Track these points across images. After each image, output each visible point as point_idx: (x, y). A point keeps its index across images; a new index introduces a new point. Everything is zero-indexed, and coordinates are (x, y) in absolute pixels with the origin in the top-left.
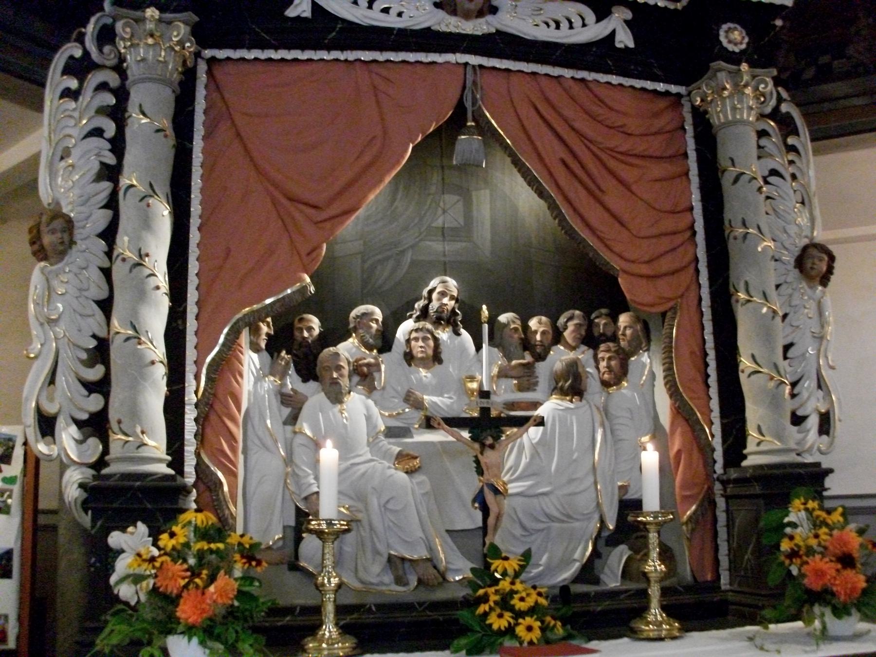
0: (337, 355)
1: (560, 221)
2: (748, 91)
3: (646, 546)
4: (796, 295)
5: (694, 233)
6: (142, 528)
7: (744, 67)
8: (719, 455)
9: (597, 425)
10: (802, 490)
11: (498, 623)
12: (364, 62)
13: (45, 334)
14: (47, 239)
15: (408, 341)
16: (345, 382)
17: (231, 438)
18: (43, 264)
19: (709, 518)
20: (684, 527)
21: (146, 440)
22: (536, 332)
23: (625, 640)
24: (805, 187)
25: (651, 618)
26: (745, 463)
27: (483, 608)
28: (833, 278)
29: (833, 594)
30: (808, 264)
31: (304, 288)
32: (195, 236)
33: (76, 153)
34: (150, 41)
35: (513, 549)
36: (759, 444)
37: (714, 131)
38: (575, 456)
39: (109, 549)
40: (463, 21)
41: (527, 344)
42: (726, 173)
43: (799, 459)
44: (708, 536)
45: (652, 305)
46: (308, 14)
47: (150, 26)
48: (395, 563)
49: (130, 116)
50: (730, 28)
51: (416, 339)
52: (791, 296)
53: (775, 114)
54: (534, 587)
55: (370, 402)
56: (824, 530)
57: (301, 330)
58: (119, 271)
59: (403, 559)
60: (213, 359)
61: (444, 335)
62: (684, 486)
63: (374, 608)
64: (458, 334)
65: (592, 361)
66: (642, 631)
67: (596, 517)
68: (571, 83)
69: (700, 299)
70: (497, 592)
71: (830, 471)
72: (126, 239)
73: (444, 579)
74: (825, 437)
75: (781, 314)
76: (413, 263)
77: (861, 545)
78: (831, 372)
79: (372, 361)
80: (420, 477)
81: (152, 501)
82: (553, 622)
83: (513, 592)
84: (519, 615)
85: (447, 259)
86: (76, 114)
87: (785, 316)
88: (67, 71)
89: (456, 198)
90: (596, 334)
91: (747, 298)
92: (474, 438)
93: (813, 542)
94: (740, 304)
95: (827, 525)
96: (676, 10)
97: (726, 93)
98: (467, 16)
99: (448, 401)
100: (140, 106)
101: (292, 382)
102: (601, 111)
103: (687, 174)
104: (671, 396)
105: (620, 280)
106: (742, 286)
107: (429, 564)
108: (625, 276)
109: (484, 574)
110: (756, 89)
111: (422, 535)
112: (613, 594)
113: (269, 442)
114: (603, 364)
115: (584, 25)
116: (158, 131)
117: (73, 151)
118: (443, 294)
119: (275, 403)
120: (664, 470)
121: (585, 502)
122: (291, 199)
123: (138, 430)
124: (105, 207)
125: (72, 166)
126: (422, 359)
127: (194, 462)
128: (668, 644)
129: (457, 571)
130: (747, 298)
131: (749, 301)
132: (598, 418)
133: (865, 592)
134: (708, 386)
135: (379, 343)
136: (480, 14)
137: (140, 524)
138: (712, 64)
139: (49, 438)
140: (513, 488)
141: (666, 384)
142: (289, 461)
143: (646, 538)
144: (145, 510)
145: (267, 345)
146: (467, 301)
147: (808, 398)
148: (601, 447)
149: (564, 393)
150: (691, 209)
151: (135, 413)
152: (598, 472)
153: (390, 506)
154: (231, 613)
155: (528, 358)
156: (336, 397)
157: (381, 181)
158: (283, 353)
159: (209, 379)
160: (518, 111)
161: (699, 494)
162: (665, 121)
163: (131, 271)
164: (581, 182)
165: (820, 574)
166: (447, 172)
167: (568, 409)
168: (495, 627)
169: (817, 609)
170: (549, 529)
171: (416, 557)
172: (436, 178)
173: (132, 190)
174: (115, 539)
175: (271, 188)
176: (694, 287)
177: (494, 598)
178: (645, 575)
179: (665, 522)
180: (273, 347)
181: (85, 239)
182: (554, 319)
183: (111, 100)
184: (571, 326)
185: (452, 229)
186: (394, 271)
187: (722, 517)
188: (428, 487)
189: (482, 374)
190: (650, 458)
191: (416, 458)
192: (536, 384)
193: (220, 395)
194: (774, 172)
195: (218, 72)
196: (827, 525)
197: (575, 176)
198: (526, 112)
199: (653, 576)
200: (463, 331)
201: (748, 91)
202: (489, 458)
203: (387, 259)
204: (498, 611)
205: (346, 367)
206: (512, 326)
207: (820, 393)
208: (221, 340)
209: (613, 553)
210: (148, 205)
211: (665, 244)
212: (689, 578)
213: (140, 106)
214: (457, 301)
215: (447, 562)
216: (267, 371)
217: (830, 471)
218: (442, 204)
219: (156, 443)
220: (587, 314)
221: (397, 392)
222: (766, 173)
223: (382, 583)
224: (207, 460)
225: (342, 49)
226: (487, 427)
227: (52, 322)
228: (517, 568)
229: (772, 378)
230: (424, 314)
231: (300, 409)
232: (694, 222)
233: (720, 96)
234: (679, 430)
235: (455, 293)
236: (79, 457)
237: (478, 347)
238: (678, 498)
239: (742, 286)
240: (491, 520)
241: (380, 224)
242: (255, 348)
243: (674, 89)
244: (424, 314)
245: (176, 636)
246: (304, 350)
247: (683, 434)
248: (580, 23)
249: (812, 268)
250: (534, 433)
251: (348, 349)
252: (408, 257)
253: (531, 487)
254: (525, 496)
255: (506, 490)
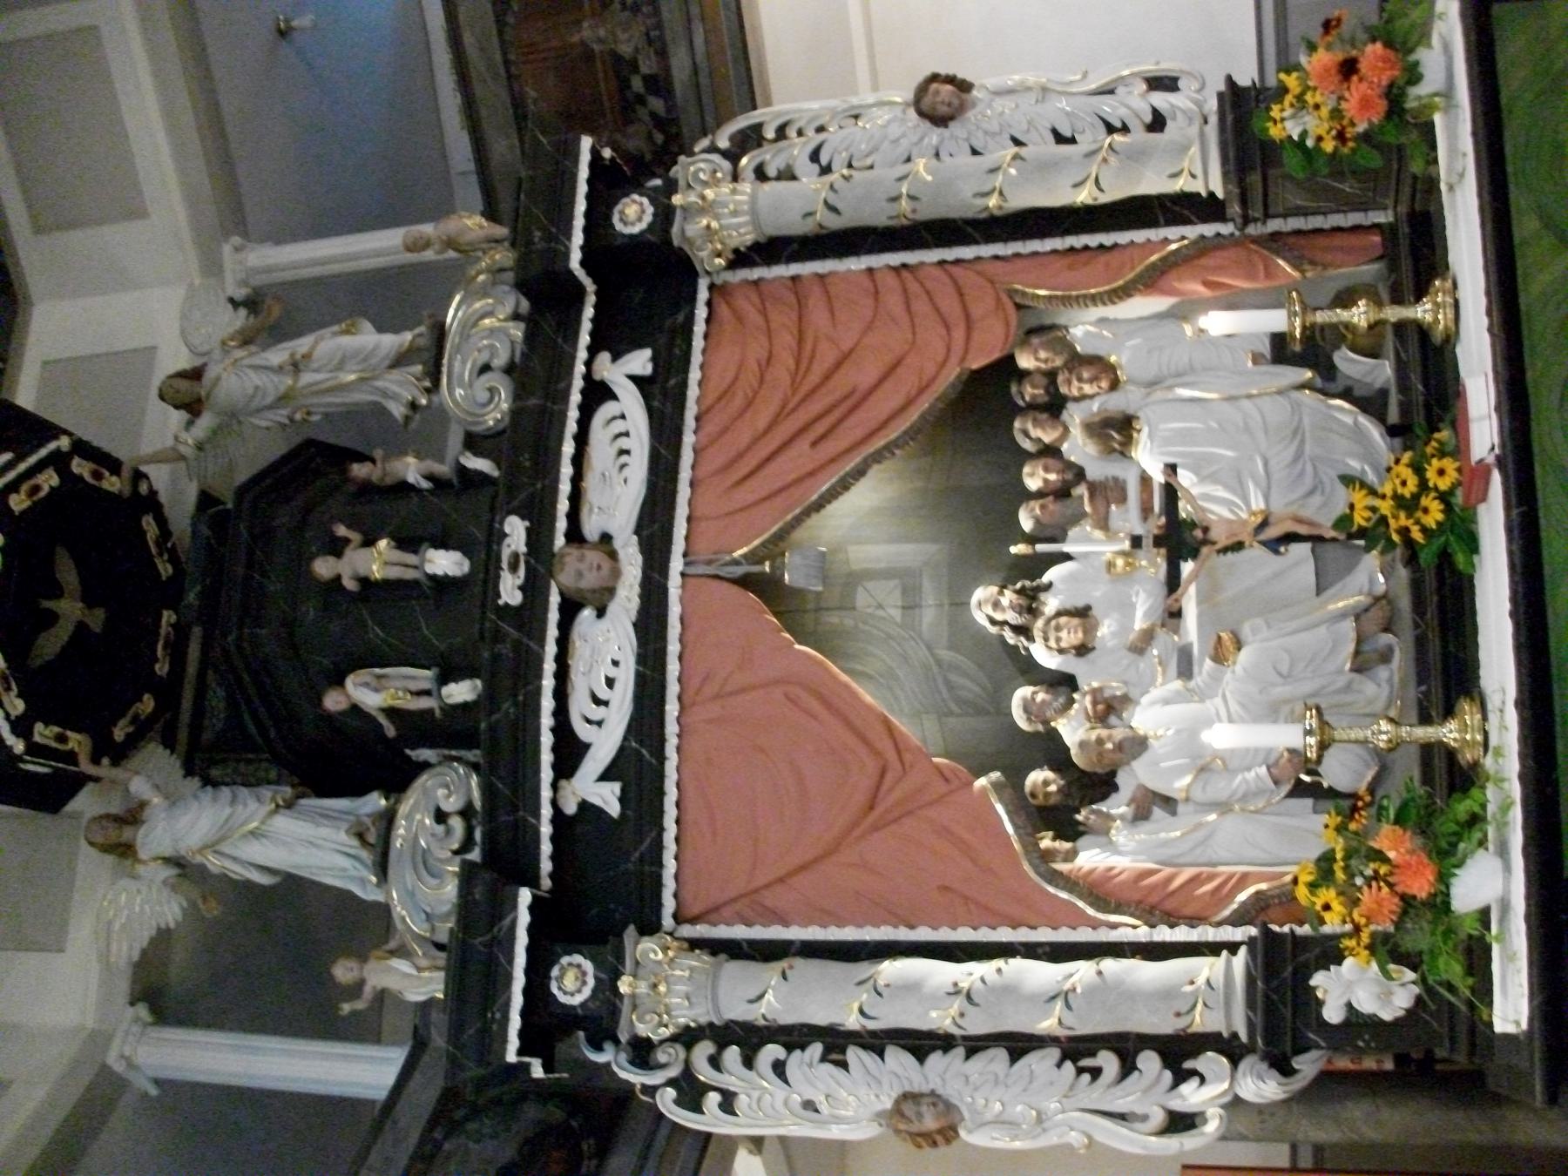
0: (1083, 745)
1: (897, 447)
2: (710, 193)
3: (1334, 327)
4: (985, 126)
5: (904, 266)
6: (1318, 979)
7: (677, 199)
8: (1208, 230)
9: (1170, 396)
10: (1256, 124)
11: (1434, 514)
12: (681, 712)
13: (1057, 1125)
14: (930, 1123)
15: (1061, 651)
16: (1119, 733)
17: (1195, 881)
18: (962, 1133)
19: (1292, 240)
20: (1309, 275)
21: (1201, 981)
22: (1046, 481)
23: (1458, 350)
24: (834, 113)
25: (1429, 318)
26: (1220, 194)
27: (1417, 535)
28: (960, 75)
29: (1391, 86)
30: (943, 110)
31: (996, 786)
32: (923, 934)
33: (810, 1094)
34: (662, 988)
35: (1341, 499)
36: (1193, 176)
37: (762, 240)
38: (1214, 425)
39: (1347, 1024)
40: (623, 579)
41: (1062, 493)
42: (825, 224)
43: (1214, 120)
44: (1321, 241)
45: (1007, 324)
46: (616, 787)
47: (643, 988)
48: (1361, 665)
49: (764, 1017)
50: (621, 220)
51: (1058, 640)
52: (986, 133)
53: (733, 156)
54: (1389, 470)
55: (1145, 700)
56: (1308, 97)
57: (1047, 795)
58: (978, 1025)
59: (1357, 653)
60: (1091, 905)
61: (1051, 604)
62: (1251, 276)
63: (1423, 688)
64: (1049, 586)
65: (1084, 404)
66: (1446, 327)
67: (1296, 395)
68: (701, 434)
69: (996, 257)
70: (1396, 517)
71: (1230, 81)
72: (934, 1014)
73: (1384, 596)
74: (1181, 84)
75: (1016, 149)
76: (952, 647)
77: (1329, 47)
78: (1091, 76)
79: (1088, 699)
80: (1246, 631)
81: (1285, 967)
82: (1434, 444)
83: (1397, 497)
84: (1423, 486)
85: (946, 601)
86: (756, 1094)
87: (1017, 142)
88: (697, 1108)
89: (860, 589)
90: (1046, 399)
91: (996, 194)
92: (1194, 554)
93: (1325, 111)
94: (1005, 205)
95: (1303, 93)
96: (597, 293)
97: (714, 224)
98: (616, 573)
99: (1142, 596)
100: (751, 1002)
101: (1118, 806)
102: (740, 394)
103: (821, 277)
104: (1130, 296)
105: (975, 366)
106: (980, 202)
107: (1363, 618)
108: (969, 357)
109: (1373, 535)
110: (705, 184)
111: (1323, 630)
112: (1401, 368)
113: (1199, 835)
114: (1088, 389)
115: (623, 417)
116: (785, 977)
117: (807, 1097)
118: (996, 605)
119: (1146, 826)
120: (1232, 303)
121: (1278, 410)
122: (871, 808)
123: (1189, 988)
124: (881, 1055)
125: (827, 1096)
126: (1085, 632)
127: (1229, 928)
128: (1461, 294)
129: (1372, 581)
130: (996, 194)
131: (1001, 193)
132: (1159, 395)
133: (1388, 44)
134: (1115, 246)
135: (1063, 689)
136: (613, 555)
137: (1312, 982)
138: (676, 243)
139: (1197, 1120)
140: (1258, 503)
141: (1114, 303)
142: (1223, 807)
143: (1323, 328)
144: (1295, 973)
145: (1067, 840)
146: (1003, 574)
147: (1128, 107)
148: (1200, 386)
149: (1128, 441)
150: (870, 270)
151: (1167, 994)
152: (1234, 392)
153: (1284, 669)
154: (1424, 829)
155: (1081, 490)
156: (1137, 745)
157: (847, 686)
158: (1079, 817)
159: (1118, 910)
160: (738, 506)
161: (1261, 255)
162: (747, 304)
163: (977, 1005)
164: (840, 421)
165: (1365, 104)
166: (823, 605)
167: (1150, 436)
168: (1440, 517)
169: (1410, 104)
170: (1314, 460)
171: (1353, 635)
172: (833, 619)
173: (866, 1009)
174: (1333, 1014)
175: (857, 833)
176: (978, 267)
177: (1404, 521)
178: (1371, 327)
179: (1302, 302)
180: (1070, 831)
181: (926, 1078)
182: (1027, 456)
183: (733, 1054)
184: (1036, 433)
185: (904, 592)
186: (966, 675)
187: (1294, 223)
188: (1259, 621)
189: (1103, 553)
190: (1218, 322)
191: (1219, 638)
192: (1116, 479)
193: (1137, 896)
194: (815, 156)
195: (695, 910)
196: (1303, 93)
197: (840, 421)
198: (747, 494)
199: (1374, 316)
200: (1045, 579)
201: (710, 193)
202: (1220, 536)
203: (947, 682)
204: (1419, 514)
205: (1098, 731)
206: (1038, 511)
207: (1121, 90)
208: (1064, 895)
209: (1348, 372)
210: (887, 986)
211: (921, 306)
212: (1376, 266)
213: (751, 1002)
214: (1003, 587)
215: (1360, 593)
216: (1103, 839)
217: (1230, 81)
218: (869, 610)
219: (1206, 968)
220: (1017, 411)
221: (1129, 665)
222: (816, 168)
223: (1390, 681)
224: (1226, 913)
225: (662, 740)
226: (1179, 539)
227: (1040, 1119)
228: (1364, 492)
229: (1105, 160)
230: (1023, 630)
231: (1155, 794)
232: (890, 267)
233: (716, 232)
234: (1177, 285)
235: (995, 589)
236: (1222, 1081)
237: (1067, 557)
238: (1268, 284)
239: (980, 202)
240: (1303, 530)
241: (899, 692)
242: (1071, 856)
243: (703, 295)
244: (1023, 630)
245: (1454, 891)
246: (1074, 789)
247: (1180, 279)
248: (620, 422)
249: (949, 105)
250: (1185, 478)
251: (1073, 731)
252: (945, 654)
253: (1257, 484)
254: (1269, 488)
255: (1262, 512)
